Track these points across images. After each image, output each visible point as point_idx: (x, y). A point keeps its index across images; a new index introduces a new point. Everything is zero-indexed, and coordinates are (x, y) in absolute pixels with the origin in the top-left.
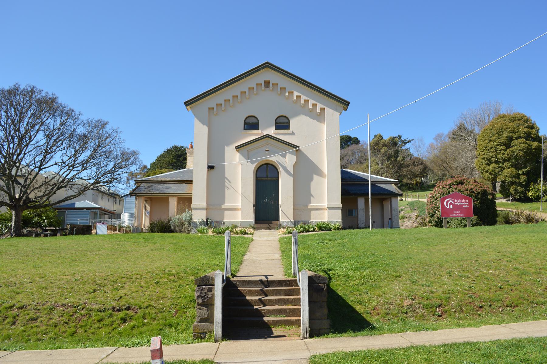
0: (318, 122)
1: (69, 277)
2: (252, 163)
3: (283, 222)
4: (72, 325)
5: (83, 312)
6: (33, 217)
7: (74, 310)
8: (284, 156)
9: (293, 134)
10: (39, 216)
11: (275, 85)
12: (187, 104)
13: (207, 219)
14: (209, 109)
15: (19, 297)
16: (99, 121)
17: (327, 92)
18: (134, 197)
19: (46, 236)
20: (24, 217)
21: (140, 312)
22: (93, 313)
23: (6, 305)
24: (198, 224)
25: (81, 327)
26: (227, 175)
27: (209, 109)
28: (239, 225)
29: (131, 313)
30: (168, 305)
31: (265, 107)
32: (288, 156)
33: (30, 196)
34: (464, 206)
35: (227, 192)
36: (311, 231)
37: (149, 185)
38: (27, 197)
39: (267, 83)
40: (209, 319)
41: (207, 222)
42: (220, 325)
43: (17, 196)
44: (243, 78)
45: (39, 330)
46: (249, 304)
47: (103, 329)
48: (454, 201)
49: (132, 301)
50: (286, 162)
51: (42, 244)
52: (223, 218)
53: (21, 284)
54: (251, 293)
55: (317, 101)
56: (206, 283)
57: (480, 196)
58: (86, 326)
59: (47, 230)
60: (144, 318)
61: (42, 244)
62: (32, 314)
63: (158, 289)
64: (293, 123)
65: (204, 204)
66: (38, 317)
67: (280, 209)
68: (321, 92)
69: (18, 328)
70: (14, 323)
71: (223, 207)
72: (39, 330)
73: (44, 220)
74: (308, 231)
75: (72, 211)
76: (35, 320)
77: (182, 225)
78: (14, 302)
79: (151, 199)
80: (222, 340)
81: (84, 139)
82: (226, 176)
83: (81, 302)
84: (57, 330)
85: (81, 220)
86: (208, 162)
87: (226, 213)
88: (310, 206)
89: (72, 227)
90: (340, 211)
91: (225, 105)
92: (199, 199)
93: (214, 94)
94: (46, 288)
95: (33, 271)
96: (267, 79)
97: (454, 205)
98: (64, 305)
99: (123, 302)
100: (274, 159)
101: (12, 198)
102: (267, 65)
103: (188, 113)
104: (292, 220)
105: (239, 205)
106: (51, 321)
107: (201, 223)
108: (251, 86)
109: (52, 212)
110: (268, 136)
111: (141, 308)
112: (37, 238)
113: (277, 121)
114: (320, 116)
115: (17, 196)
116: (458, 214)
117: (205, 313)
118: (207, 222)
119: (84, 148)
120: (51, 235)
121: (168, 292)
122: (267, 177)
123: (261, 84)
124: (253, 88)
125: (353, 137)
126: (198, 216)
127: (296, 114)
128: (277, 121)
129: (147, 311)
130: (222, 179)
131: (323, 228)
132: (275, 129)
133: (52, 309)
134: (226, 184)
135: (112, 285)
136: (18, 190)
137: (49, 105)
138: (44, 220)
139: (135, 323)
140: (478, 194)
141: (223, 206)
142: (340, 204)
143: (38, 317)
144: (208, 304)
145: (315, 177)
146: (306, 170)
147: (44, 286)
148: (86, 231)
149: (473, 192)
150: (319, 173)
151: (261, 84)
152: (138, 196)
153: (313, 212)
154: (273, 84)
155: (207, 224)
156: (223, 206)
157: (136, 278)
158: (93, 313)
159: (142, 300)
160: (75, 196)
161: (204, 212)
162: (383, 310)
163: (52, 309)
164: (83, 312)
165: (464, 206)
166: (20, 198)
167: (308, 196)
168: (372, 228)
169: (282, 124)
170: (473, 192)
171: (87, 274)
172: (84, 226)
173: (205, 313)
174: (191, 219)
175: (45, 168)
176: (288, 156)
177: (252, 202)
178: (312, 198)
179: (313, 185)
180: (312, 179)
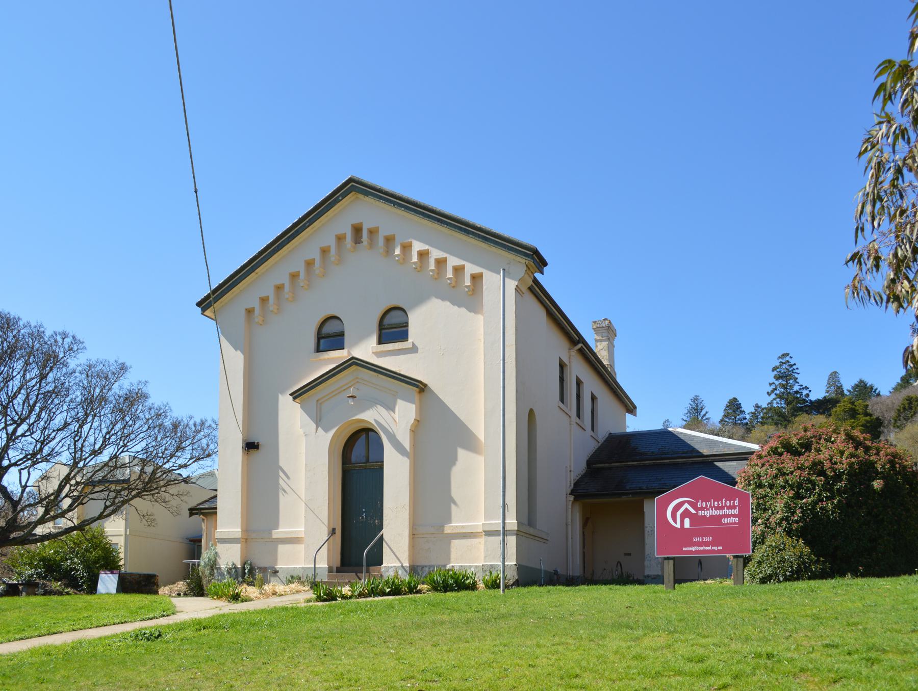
0: (470, 311)
2: (326, 430)
3: (388, 568)
8: (391, 408)
9: (414, 349)
11: (372, 232)
17: (480, 229)
26: (282, 463)
31: (354, 293)
32: (401, 404)
34: (725, 521)
35: (283, 500)
41: (244, 569)
50: (396, 420)
52: (276, 563)
55: (464, 260)
57: (841, 485)
64: (417, 321)
65: (236, 530)
68: (468, 233)
71: (274, 536)
82: (281, 464)
87: (282, 548)
88: (448, 529)
97: (694, 519)
100: (371, 416)
102: (353, 187)
104: (406, 564)
105: (299, 529)
113: (387, 321)
114: (469, 295)
118: (244, 569)
122: (368, 461)
127: (420, 300)
130: (275, 469)
132: (380, 342)
134: (281, 482)
140: (838, 477)
141: (276, 534)
145: (462, 453)
146: (441, 434)
148: (145, 585)
149: (822, 473)
150: (467, 440)
153: (456, 544)
156: (276, 534)
160: (101, 517)
165: (725, 521)
167: (446, 502)
169: (392, 329)
170: (822, 473)
172: (140, 575)
174: (215, 563)
176: (401, 404)
177: (326, 522)
178: (453, 506)
179: (457, 473)
180: (453, 460)
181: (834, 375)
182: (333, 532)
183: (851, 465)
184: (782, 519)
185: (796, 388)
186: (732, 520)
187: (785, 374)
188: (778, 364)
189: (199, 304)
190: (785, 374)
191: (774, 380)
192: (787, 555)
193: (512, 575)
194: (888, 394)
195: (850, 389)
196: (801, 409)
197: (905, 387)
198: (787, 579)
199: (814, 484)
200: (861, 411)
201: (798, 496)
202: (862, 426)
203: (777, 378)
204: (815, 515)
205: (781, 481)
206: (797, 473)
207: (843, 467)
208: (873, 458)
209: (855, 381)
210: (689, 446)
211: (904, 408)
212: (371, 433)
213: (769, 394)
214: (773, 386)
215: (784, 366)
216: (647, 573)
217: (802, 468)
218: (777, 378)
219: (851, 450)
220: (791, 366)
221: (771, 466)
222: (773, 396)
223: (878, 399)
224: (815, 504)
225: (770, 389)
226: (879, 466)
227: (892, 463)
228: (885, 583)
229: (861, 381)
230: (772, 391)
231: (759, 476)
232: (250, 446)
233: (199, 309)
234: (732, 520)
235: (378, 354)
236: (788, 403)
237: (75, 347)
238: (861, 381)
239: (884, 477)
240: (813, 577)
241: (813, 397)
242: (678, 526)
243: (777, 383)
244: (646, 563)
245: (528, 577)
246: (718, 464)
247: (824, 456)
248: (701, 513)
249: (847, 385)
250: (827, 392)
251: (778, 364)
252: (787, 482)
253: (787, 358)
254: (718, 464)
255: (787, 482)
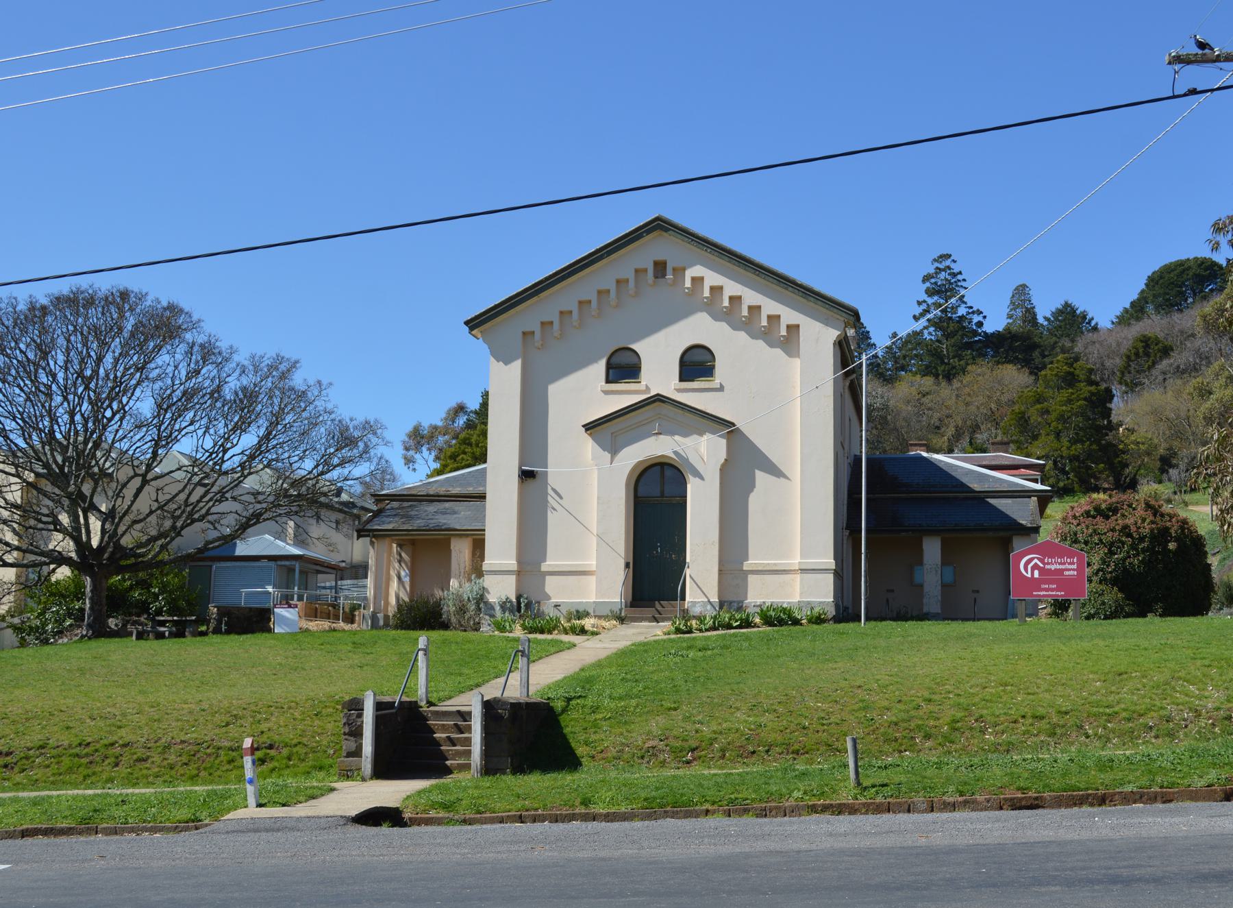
1: (193, 706)
3: (694, 603)
4: (193, 766)
5: (208, 751)
6: (131, 588)
7: (196, 748)
9: (721, 388)
10: (145, 585)
12: (474, 324)
13: (519, 597)
14: (524, 333)
15: (123, 732)
16: (280, 359)
18: (368, 539)
19: (160, 636)
20: (109, 589)
21: (285, 752)
22: (222, 752)
23: (106, 742)
24: (498, 608)
25: (205, 769)
27: (524, 333)
28: (591, 611)
29: (272, 752)
30: (325, 743)
33: (123, 542)
34: (1067, 573)
36: (736, 628)
37: (406, 504)
38: (118, 546)
39: (660, 268)
40: (357, 753)
41: (519, 603)
42: (369, 760)
43: (95, 543)
44: (601, 258)
45: (150, 772)
46: (437, 743)
47: (234, 772)
48: (1042, 561)
49: (276, 738)
51: (153, 656)
53: (124, 715)
54: (444, 728)
56: (355, 706)
58: (211, 767)
59: (163, 623)
60: (289, 759)
61: (153, 656)
62: (140, 753)
63: (317, 722)
65: (511, 563)
66: (148, 757)
67: (688, 572)
69: (123, 770)
70: (117, 765)
72: (150, 772)
73: (156, 596)
74: (729, 627)
75: (229, 564)
76: (145, 760)
77: (462, 610)
78: (115, 738)
79: (413, 543)
80: (371, 779)
81: (247, 401)
83: (207, 738)
84: (173, 772)
85: (246, 594)
86: (521, 464)
89: (224, 612)
90: (830, 578)
91: (561, 322)
92: (501, 552)
93: (535, 299)
94: (159, 720)
95: (140, 698)
96: (660, 258)
98: (183, 742)
99: (264, 738)
101: (83, 547)
102: (659, 225)
103: (477, 346)
104: (715, 599)
105: (592, 563)
106: (165, 763)
107: (503, 606)
108: (603, 287)
109: (176, 575)
110: (659, 399)
111: (286, 746)
112: (142, 643)
113: (686, 358)
114: (789, 341)
115: (95, 543)
116: (1052, 590)
117: (351, 745)
118: (519, 603)
119: (241, 427)
120: (174, 635)
121: (330, 726)
122: (662, 496)
123: (646, 270)
124: (627, 281)
125: (1135, 297)
126: (500, 589)
128: (686, 358)
129: (295, 750)
131: (780, 618)
132: (681, 380)
133: (167, 747)
135: (253, 717)
136: (95, 524)
137: (165, 325)
138: (156, 596)
139: (276, 764)
140: (1142, 539)
142: (829, 561)
143: (148, 757)
144: (357, 733)
147: (156, 717)
149: (1129, 535)
151: (646, 270)
152: (374, 536)
154: (674, 269)
155: (519, 610)
157: (290, 708)
158: (222, 752)
159: (290, 736)
161: (512, 579)
162: (613, 752)
163: (167, 747)
164: (208, 751)
165: (1067, 573)
166: (101, 548)
168: (867, 619)
170: (1129, 535)
171: (220, 702)
173: (351, 745)
174: (482, 596)
175: (156, 478)
181: (1022, 290)
182: (627, 565)
183: (1152, 530)
184: (1098, 570)
185: (962, 311)
186: (1072, 573)
187: (944, 285)
188: (932, 271)
189: (467, 323)
190: (944, 285)
191: (925, 297)
192: (1106, 598)
193: (831, 612)
194: (1109, 326)
195: (1049, 315)
196: (969, 346)
197: (1138, 319)
198: (1106, 618)
199: (1123, 543)
200: (1082, 377)
201: (1111, 553)
202: (1085, 399)
203: (930, 293)
204: (1125, 568)
205: (1096, 539)
206: (1110, 534)
207: (1146, 530)
208: (1168, 524)
209: (1058, 304)
210: (963, 485)
211: (1137, 354)
212: (668, 472)
213: (916, 318)
214: (924, 307)
215: (943, 275)
216: (925, 610)
217: (1113, 530)
218: (930, 293)
219: (1152, 518)
220: (954, 275)
221: (1087, 528)
222: (923, 322)
223: (1095, 336)
224: (1124, 560)
225: (918, 310)
226: (1173, 531)
227: (1182, 528)
228: (1191, 619)
229: (1067, 305)
230: (922, 315)
231: (1075, 534)
232: (527, 476)
233: (467, 329)
234: (1072, 573)
235: (679, 390)
236: (948, 336)
237: (195, 326)
238: (1067, 305)
239: (1177, 540)
240: (1128, 616)
241: (991, 326)
242: (1029, 575)
243: (930, 301)
244: (925, 601)
245: (845, 613)
246: (992, 501)
247: (1130, 521)
248: (1048, 567)
249: (1044, 310)
250: (1010, 317)
251: (932, 271)
252: (1101, 540)
253: (948, 262)
254: (992, 501)
255: (1101, 540)
